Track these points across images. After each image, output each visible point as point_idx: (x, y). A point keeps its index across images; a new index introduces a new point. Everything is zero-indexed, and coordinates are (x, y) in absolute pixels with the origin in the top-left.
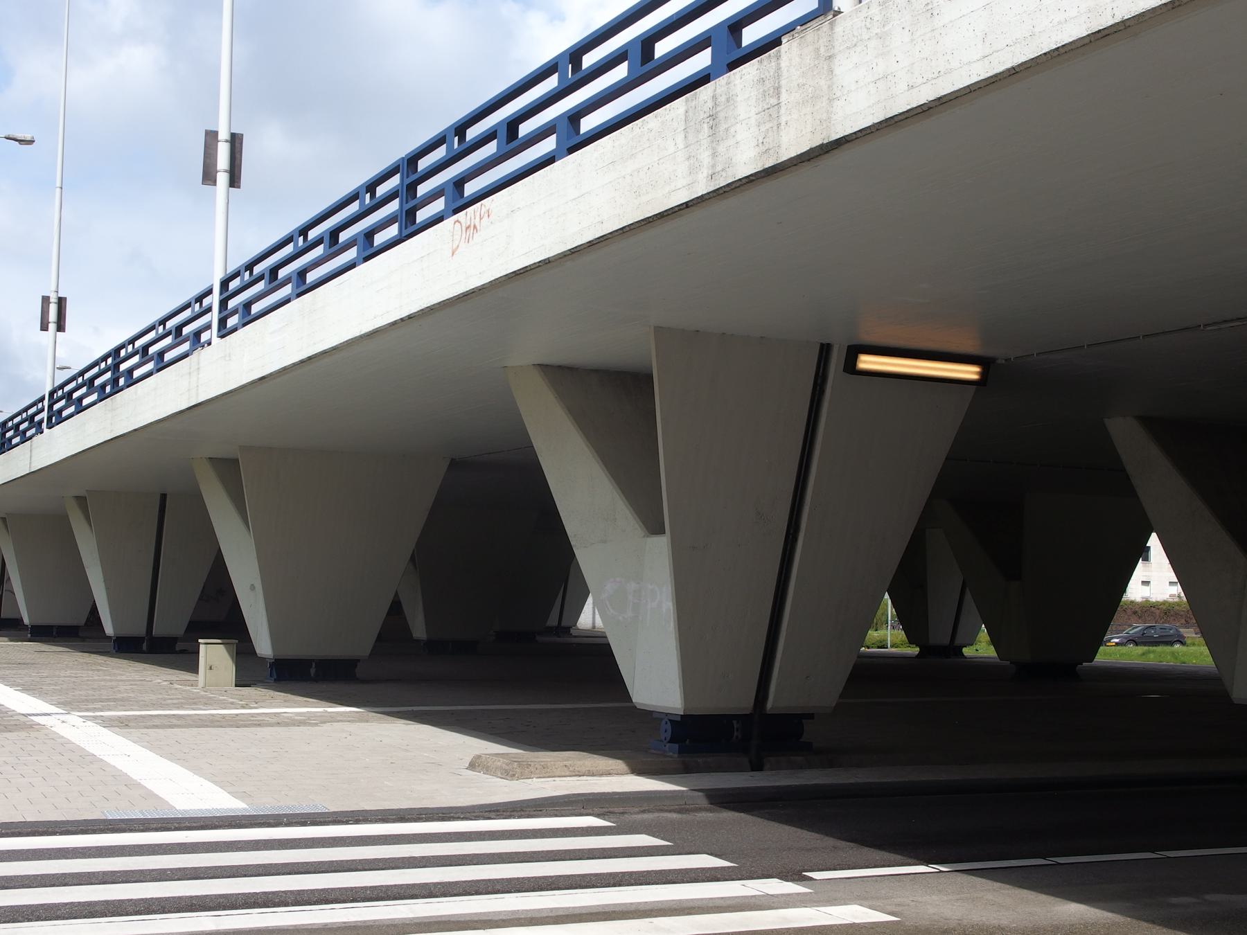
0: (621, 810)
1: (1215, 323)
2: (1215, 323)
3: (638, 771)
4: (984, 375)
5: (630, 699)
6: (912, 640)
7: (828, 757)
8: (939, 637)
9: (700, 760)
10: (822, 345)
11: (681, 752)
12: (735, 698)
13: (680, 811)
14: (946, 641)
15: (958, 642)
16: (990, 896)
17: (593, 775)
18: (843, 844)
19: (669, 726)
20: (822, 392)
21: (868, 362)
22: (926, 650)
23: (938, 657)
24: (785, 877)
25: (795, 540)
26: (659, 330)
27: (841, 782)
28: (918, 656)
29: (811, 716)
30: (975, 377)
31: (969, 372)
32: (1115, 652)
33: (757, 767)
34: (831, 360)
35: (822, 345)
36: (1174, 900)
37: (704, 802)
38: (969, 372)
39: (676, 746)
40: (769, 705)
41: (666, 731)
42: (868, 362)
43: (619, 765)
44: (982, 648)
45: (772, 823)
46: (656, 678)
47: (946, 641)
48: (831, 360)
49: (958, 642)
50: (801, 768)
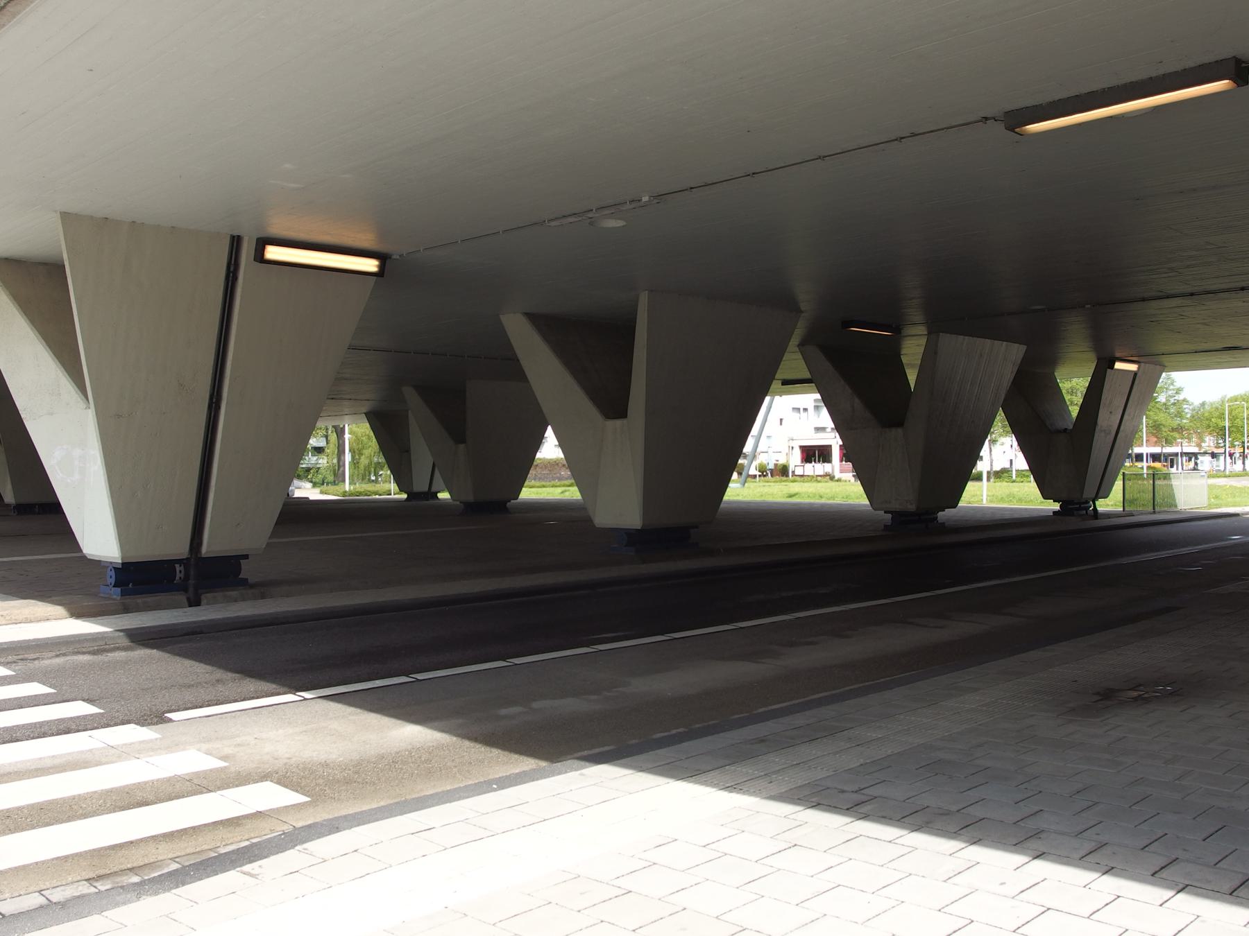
0: (37, 655)
1: (557, 219)
2: (557, 219)
3: (77, 614)
4: (382, 267)
5: (81, 551)
6: (401, 490)
7: (262, 589)
8: (421, 486)
9: (139, 601)
10: (233, 237)
11: (123, 594)
12: (171, 544)
13: (94, 653)
14: (426, 489)
15: (433, 489)
16: (335, 725)
17: (31, 622)
18: (230, 675)
19: (113, 573)
20: (235, 278)
21: (273, 253)
22: (412, 496)
23: (420, 498)
24: (143, 721)
25: (218, 408)
26: (66, 217)
27: (272, 611)
28: (407, 500)
29: (246, 557)
30: (375, 269)
31: (370, 265)
32: (738, 492)
33: (195, 602)
34: (240, 252)
35: (233, 237)
36: (503, 712)
37: (125, 642)
38: (370, 265)
39: (119, 590)
40: (204, 550)
41: (111, 578)
42: (273, 253)
43: (59, 610)
44: (444, 495)
45: (178, 659)
46: (98, 534)
47: (426, 489)
48: (240, 252)
49: (433, 489)
50: (236, 601)
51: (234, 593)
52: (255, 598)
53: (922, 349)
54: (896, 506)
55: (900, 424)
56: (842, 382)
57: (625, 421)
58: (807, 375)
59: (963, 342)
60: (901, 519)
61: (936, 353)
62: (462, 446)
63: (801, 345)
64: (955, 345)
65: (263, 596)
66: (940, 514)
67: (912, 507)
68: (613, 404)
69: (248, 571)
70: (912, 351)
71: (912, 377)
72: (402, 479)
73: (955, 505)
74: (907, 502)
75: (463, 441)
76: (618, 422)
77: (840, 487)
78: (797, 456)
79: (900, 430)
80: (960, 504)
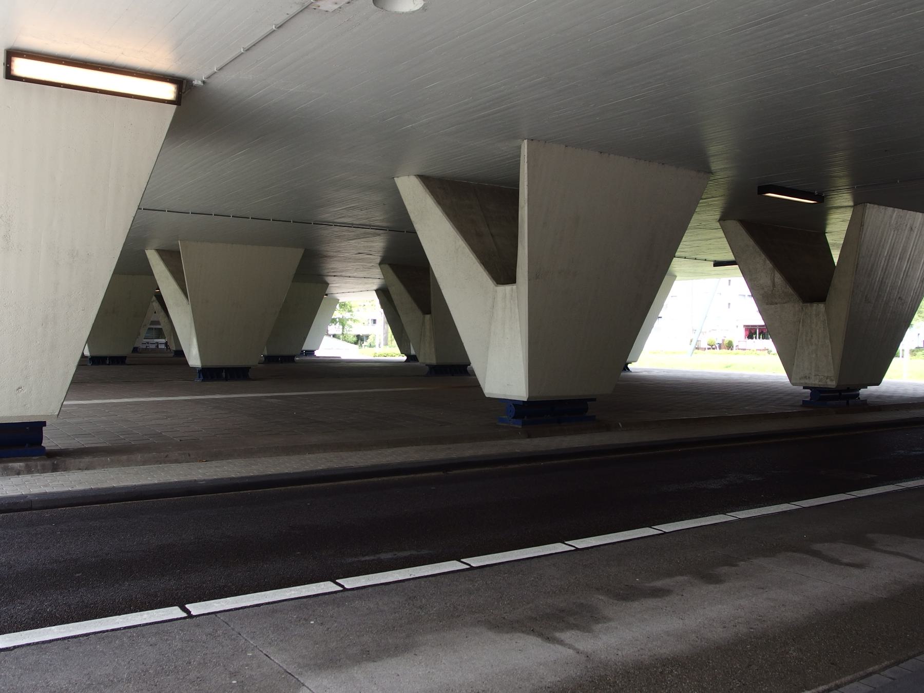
7: (57, 459)
28: (406, 361)
38: (168, 91)
42: (21, 67)
50: (18, 474)
51: (18, 465)
52: (44, 470)
53: (846, 228)
54: (815, 382)
55: (821, 299)
56: (763, 256)
57: (514, 287)
58: (730, 257)
59: (893, 214)
60: (820, 395)
61: (862, 225)
62: (428, 317)
63: (878, 384)
64: (884, 218)
65: (55, 469)
66: (862, 390)
67: (832, 384)
68: (502, 271)
69: (49, 441)
70: (836, 231)
71: (836, 255)
72: (403, 348)
73: (878, 383)
74: (827, 377)
75: (429, 312)
76: (508, 288)
77: (384, 348)
78: (742, 333)
79: (822, 306)
80: (885, 379)
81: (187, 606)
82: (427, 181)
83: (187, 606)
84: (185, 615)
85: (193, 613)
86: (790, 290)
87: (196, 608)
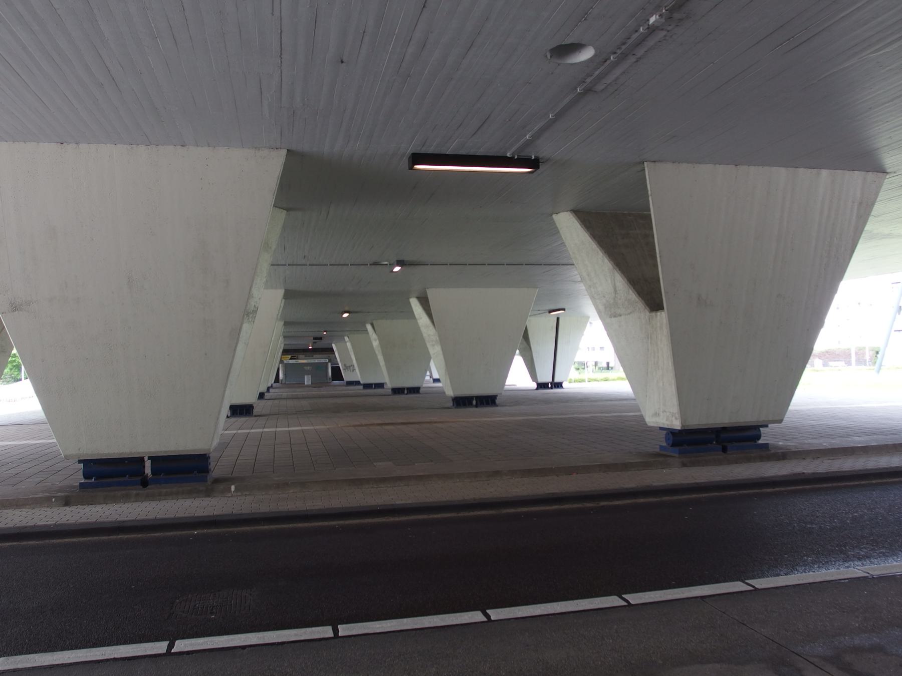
81: (488, 611)
82: (578, 213)
83: (488, 611)
84: (485, 619)
85: (492, 618)
86: (633, 296)
87: (496, 614)
